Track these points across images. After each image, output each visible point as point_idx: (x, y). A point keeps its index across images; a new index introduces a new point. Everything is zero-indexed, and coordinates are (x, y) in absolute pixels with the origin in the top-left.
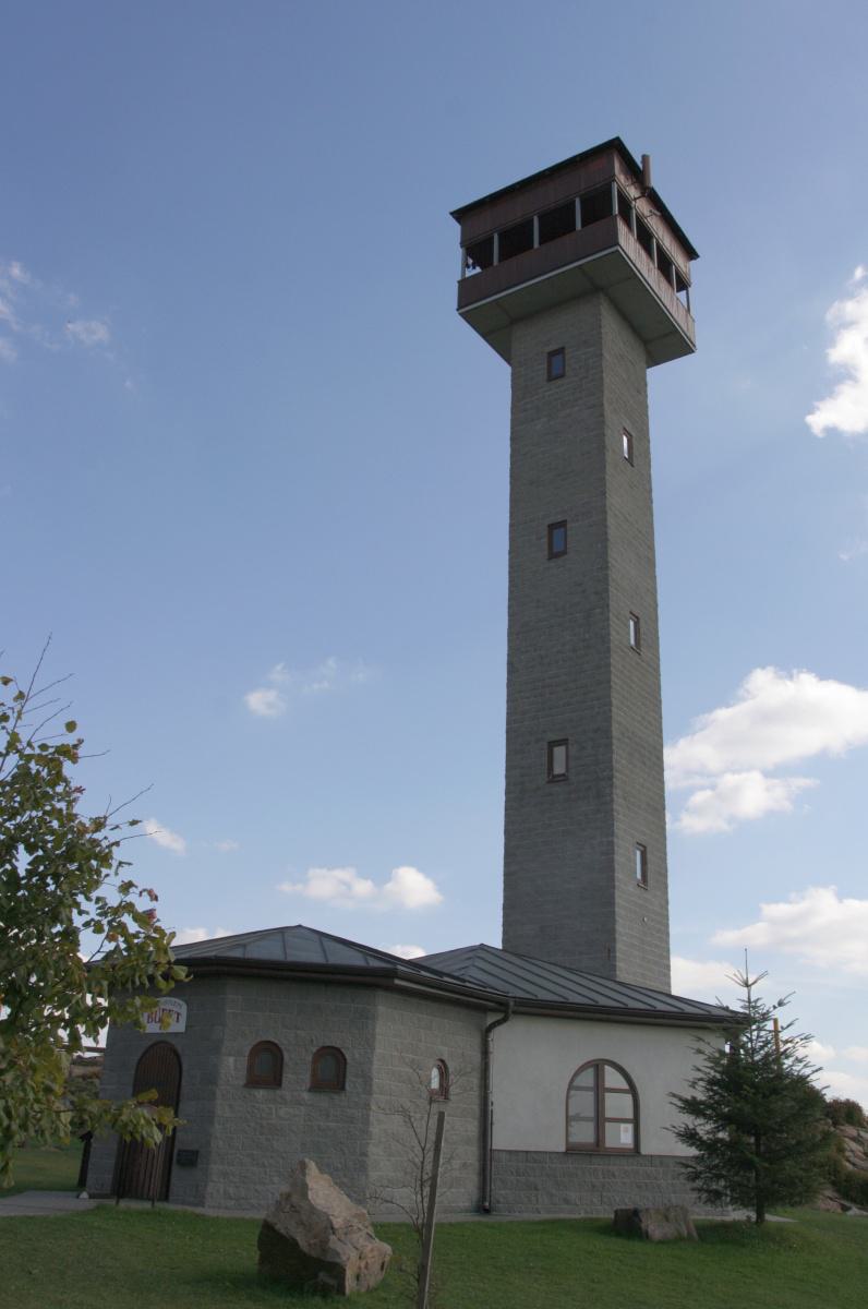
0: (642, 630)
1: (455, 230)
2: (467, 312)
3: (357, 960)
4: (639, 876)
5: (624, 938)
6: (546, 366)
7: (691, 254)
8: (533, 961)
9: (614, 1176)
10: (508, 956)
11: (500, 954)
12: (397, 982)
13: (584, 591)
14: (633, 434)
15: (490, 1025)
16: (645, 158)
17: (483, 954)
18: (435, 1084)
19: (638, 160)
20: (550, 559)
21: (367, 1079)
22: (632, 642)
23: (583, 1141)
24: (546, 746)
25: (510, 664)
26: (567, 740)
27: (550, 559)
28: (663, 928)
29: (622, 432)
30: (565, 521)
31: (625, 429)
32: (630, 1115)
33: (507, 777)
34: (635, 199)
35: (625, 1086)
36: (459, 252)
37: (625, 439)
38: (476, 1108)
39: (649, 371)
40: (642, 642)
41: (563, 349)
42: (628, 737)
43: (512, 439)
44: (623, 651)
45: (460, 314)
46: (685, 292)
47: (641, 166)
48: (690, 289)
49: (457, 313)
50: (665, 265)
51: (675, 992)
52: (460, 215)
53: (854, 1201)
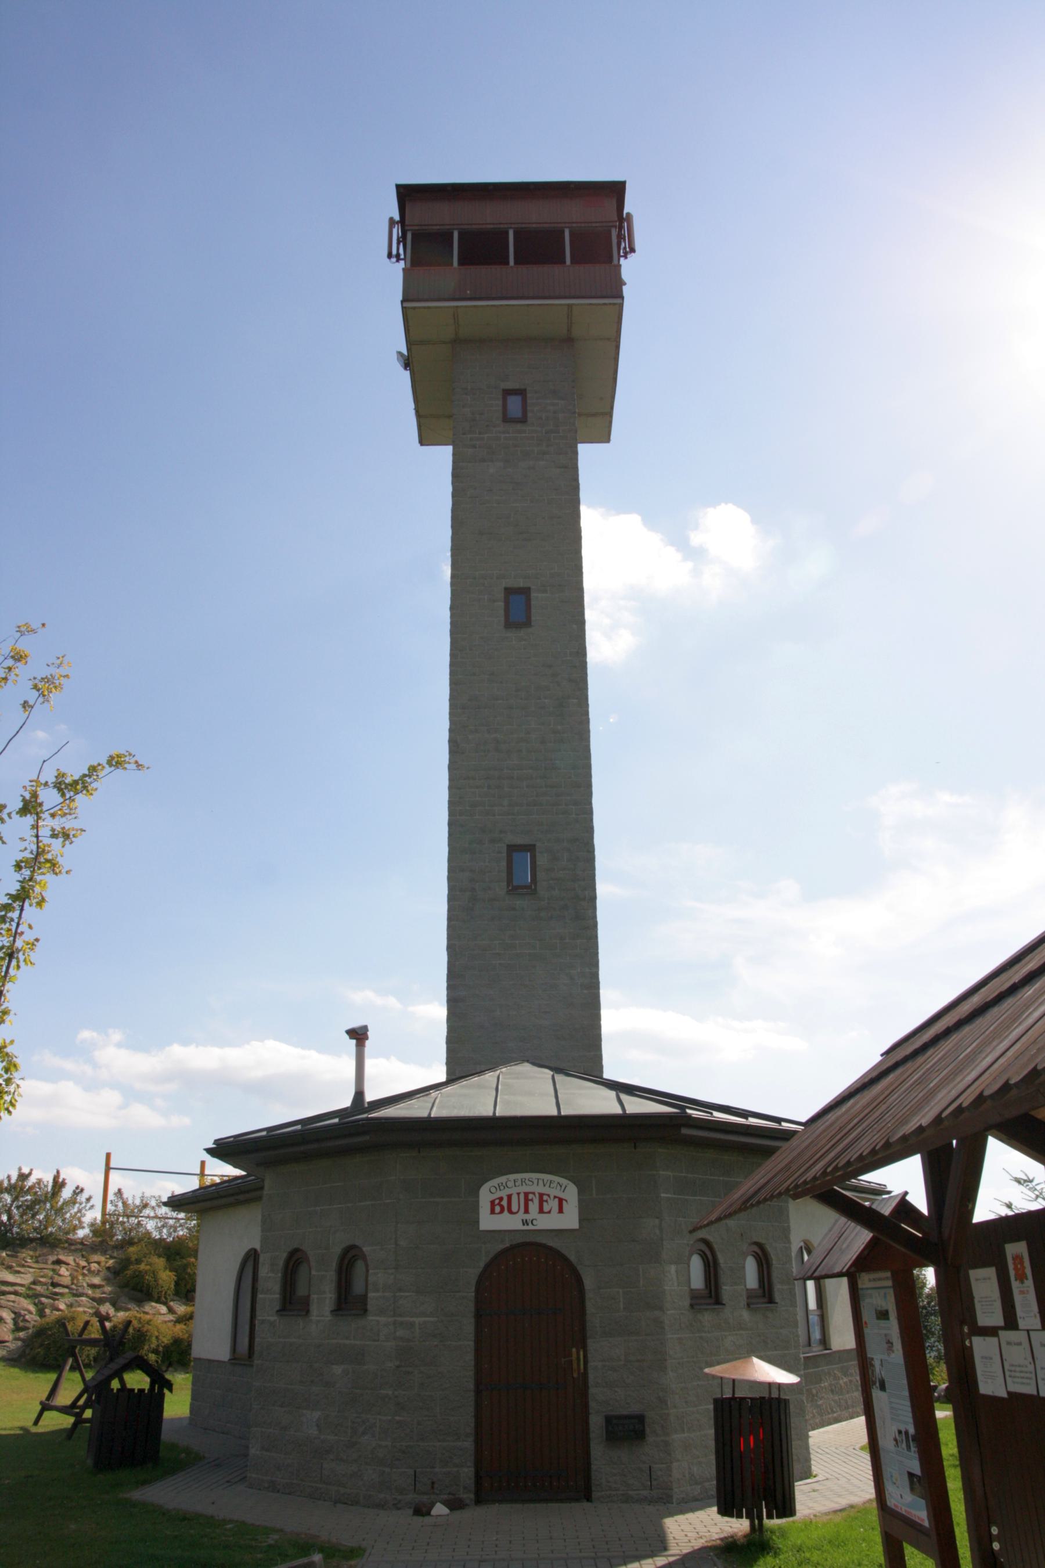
52: (407, 194)
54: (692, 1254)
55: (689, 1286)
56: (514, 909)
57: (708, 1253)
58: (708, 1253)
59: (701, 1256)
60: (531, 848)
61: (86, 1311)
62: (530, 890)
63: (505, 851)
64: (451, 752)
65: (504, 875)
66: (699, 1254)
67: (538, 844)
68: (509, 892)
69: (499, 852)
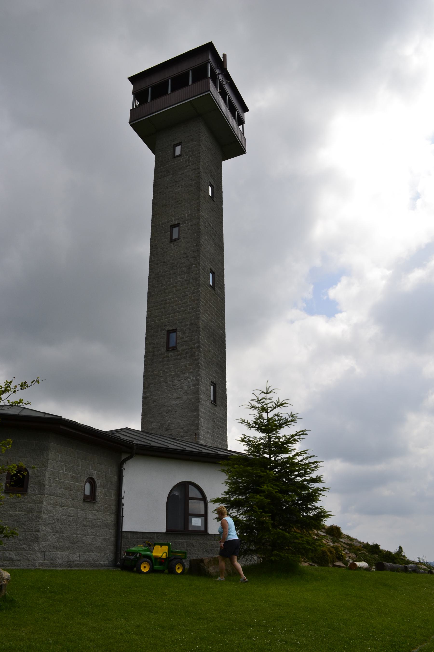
0: (216, 279)
1: (130, 86)
2: (134, 124)
3: (42, 415)
4: (212, 398)
5: (204, 429)
6: (172, 151)
7: (246, 109)
8: (153, 435)
9: (193, 546)
10: (142, 433)
11: (140, 433)
12: (61, 427)
13: (187, 257)
14: (215, 187)
15: (123, 460)
16: (224, 55)
17: (125, 430)
18: (87, 492)
19: (221, 57)
20: (170, 242)
21: (42, 486)
22: (211, 284)
23: (29, 415)
24: (165, 332)
25: (149, 293)
26: (177, 329)
27: (170, 242)
28: (224, 426)
29: (209, 183)
30: (179, 224)
31: (210, 183)
32: (203, 512)
33: (146, 349)
34: (219, 74)
35: (200, 496)
36: (132, 96)
37: (211, 275)
38: (114, 508)
39: (224, 163)
40: (216, 284)
41: (181, 142)
42: (208, 329)
43: (154, 186)
44: (206, 287)
45: (130, 125)
46: (242, 126)
47: (222, 59)
48: (244, 125)
49: (129, 124)
50: (232, 110)
51: (228, 449)
52: (133, 79)
53: (316, 563)
54: (86, 482)
55: (84, 493)
56: (168, 357)
57: (93, 482)
58: (93, 482)
59: (90, 483)
60: (175, 331)
61: (190, 555)
62: (175, 348)
63: (166, 333)
64: (148, 297)
65: (165, 344)
66: (89, 482)
67: (178, 328)
68: (167, 351)
69: (164, 334)
